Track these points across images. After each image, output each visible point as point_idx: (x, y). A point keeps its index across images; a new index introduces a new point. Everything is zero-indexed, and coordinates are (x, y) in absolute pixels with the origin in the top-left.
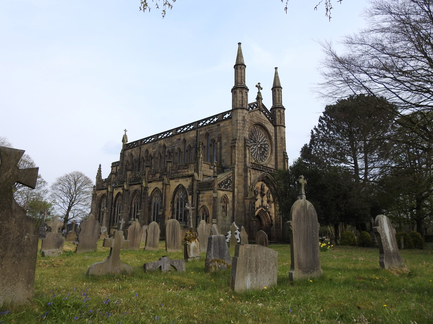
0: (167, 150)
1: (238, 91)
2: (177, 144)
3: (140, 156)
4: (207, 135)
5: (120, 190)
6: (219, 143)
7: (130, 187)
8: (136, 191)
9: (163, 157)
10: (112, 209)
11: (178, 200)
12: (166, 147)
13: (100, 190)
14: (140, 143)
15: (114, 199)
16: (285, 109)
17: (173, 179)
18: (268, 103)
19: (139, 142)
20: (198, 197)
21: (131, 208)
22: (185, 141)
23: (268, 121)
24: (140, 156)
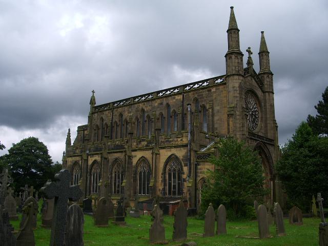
0: (146, 115)
1: (233, 57)
2: (158, 109)
3: (112, 120)
4: (196, 100)
5: (97, 158)
6: (210, 110)
7: (109, 155)
8: (116, 159)
9: (141, 122)
10: (87, 178)
11: (170, 170)
12: (144, 111)
13: (71, 156)
14: (110, 107)
15: (89, 167)
16: (273, 74)
17: (163, 148)
18: (257, 68)
19: (111, 105)
20: (196, 168)
21: (111, 178)
22: (168, 105)
23: (257, 86)
24: (112, 120)
